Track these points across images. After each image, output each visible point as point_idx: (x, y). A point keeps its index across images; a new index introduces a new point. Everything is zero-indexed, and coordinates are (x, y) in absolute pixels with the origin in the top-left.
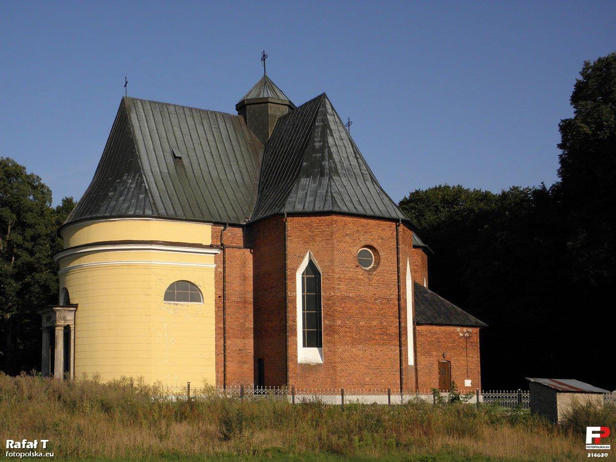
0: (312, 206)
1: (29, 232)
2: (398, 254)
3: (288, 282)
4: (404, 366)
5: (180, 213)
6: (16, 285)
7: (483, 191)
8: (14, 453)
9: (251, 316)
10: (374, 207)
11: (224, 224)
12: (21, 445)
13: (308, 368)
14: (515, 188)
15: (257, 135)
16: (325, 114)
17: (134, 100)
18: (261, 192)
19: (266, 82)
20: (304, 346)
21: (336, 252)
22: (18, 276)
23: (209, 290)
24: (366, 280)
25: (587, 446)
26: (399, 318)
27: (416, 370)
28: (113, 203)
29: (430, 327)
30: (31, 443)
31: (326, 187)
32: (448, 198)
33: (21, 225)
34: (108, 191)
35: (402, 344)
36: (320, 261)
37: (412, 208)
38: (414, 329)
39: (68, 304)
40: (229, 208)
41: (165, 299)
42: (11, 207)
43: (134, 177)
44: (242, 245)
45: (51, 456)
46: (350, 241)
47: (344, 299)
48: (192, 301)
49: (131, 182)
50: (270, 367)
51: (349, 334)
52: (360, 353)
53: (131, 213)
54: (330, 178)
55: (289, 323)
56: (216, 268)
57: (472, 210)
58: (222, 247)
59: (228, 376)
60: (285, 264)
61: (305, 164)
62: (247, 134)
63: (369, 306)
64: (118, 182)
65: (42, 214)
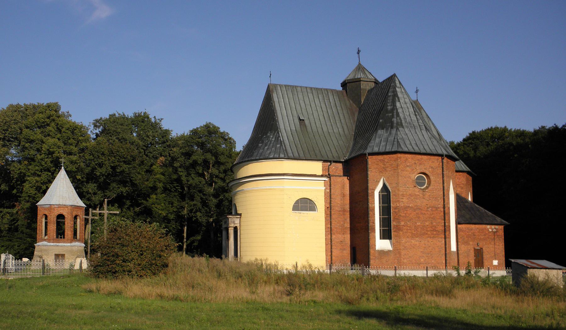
0: (384, 148)
1: (222, 168)
2: (443, 177)
3: (370, 198)
4: (448, 251)
5: (302, 155)
6: (215, 201)
7: (521, 130)
9: (348, 220)
10: (426, 147)
11: (330, 162)
13: (383, 253)
14: (543, 127)
15: (354, 103)
16: (395, 87)
17: (275, 86)
18: (355, 139)
19: (360, 68)
20: (381, 239)
21: (400, 178)
22: (216, 196)
23: (321, 203)
24: (421, 195)
26: (444, 220)
27: (458, 253)
28: (261, 151)
29: (468, 226)
31: (394, 135)
32: (496, 135)
33: (218, 163)
34: (259, 143)
35: (446, 237)
36: (390, 184)
37: (471, 143)
38: (456, 227)
39: (237, 214)
40: (333, 150)
41: (293, 210)
42: (211, 153)
43: (274, 134)
44: (342, 174)
46: (410, 170)
47: (406, 208)
48: (310, 210)
49: (272, 138)
50: (360, 252)
51: (409, 231)
52: (417, 243)
53: (272, 156)
54: (397, 129)
55: (371, 224)
56: (325, 190)
57: (512, 144)
58: (329, 176)
59: (333, 258)
60: (367, 186)
61: (381, 121)
62: (347, 102)
63: (423, 212)
64: (266, 137)
65: (230, 156)
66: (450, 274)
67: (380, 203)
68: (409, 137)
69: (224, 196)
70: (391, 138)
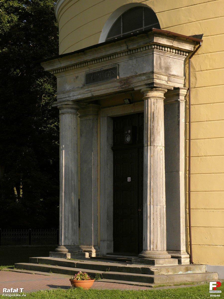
8: (7, 295)
12: (10, 291)
25: (210, 291)
30: (15, 290)
45: (25, 296)
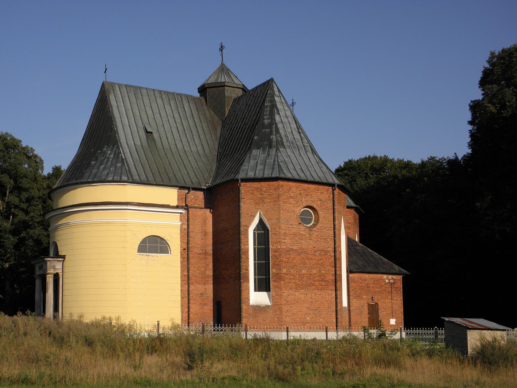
1: (24, 195)
3: (242, 237)
5: (151, 179)
6: (13, 240)
7: (406, 160)
9: (211, 266)
10: (314, 174)
11: (188, 189)
13: (259, 309)
14: (432, 158)
17: (112, 85)
18: (219, 161)
19: (223, 69)
20: (255, 291)
21: (282, 212)
24: (307, 235)
26: (335, 267)
27: (349, 310)
28: (95, 171)
29: (361, 275)
31: (273, 157)
32: (376, 166)
33: (18, 189)
35: (337, 290)
36: (269, 219)
38: (348, 277)
39: (57, 255)
40: (192, 175)
41: (139, 251)
42: (9, 174)
43: (112, 149)
44: (203, 206)
46: (294, 202)
47: (289, 251)
48: (161, 252)
49: (110, 153)
50: (227, 307)
51: (293, 281)
52: (302, 296)
53: (110, 179)
54: (277, 149)
55: (243, 271)
56: (181, 225)
57: (396, 177)
58: (187, 208)
59: (191, 315)
60: (239, 222)
61: (256, 138)
62: (207, 112)
63: (309, 256)
64: (99, 153)
66: (355, 338)
67: (254, 245)
68: (292, 160)
69: (28, 233)
70: (270, 161)
